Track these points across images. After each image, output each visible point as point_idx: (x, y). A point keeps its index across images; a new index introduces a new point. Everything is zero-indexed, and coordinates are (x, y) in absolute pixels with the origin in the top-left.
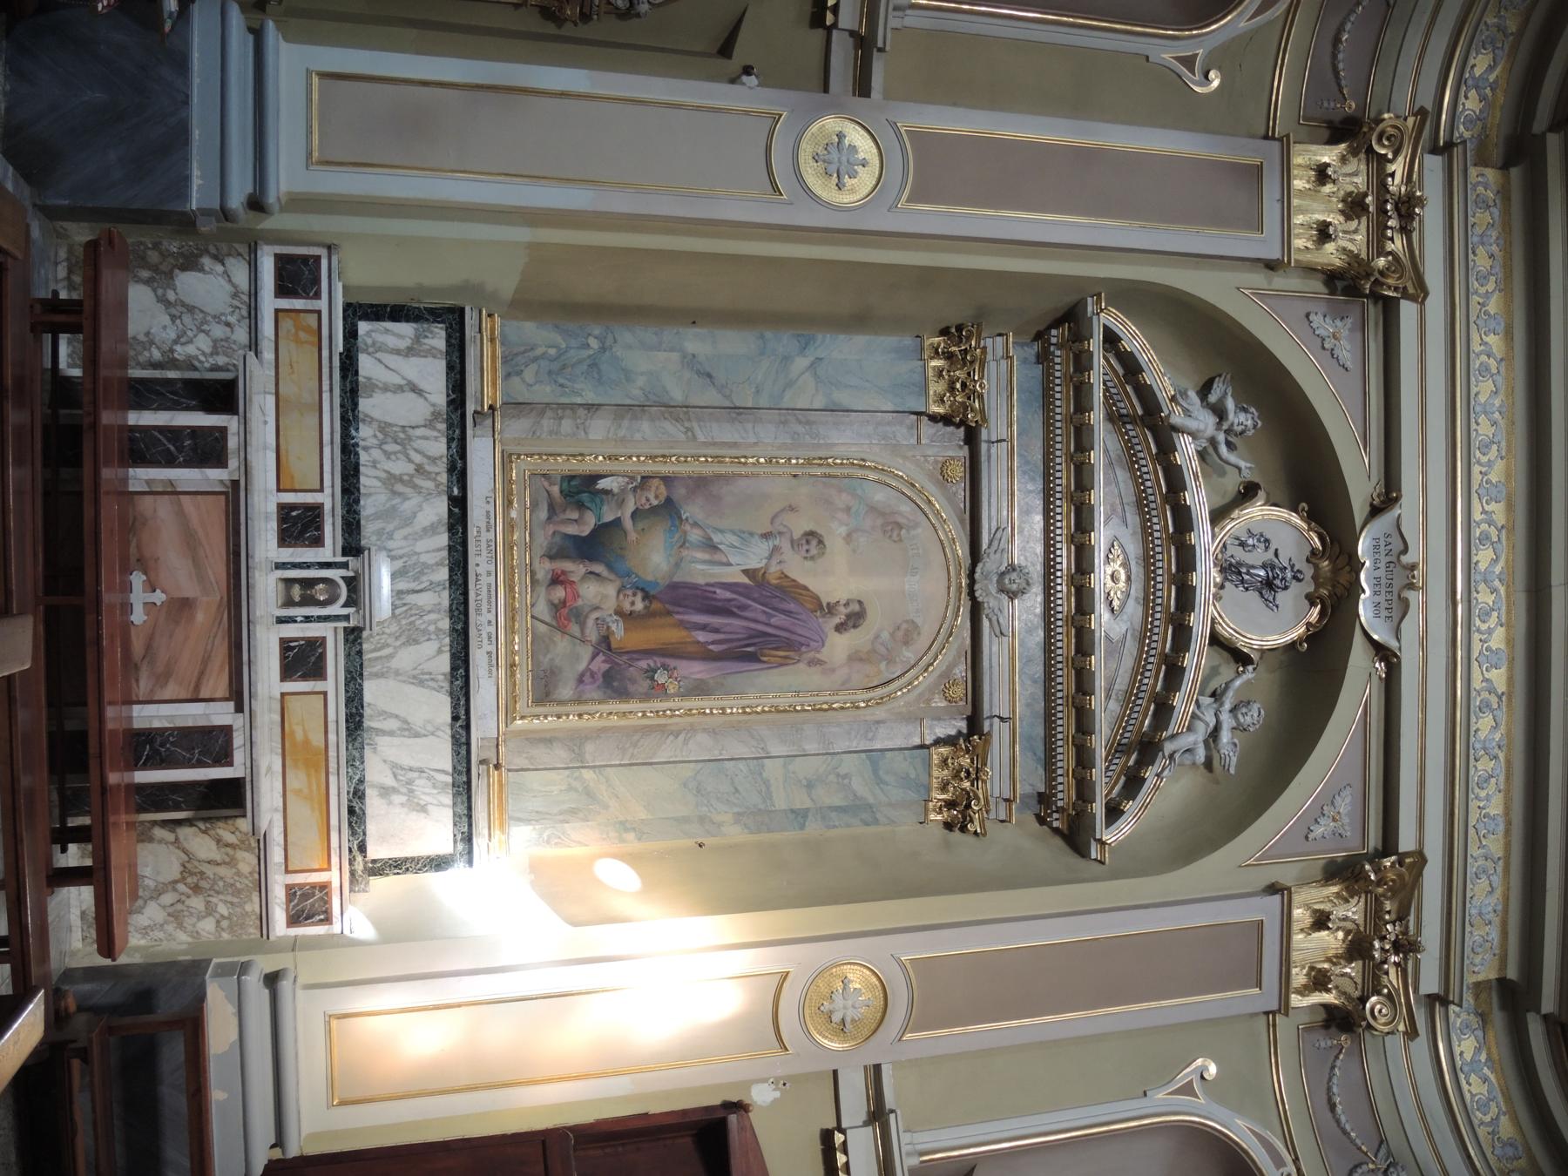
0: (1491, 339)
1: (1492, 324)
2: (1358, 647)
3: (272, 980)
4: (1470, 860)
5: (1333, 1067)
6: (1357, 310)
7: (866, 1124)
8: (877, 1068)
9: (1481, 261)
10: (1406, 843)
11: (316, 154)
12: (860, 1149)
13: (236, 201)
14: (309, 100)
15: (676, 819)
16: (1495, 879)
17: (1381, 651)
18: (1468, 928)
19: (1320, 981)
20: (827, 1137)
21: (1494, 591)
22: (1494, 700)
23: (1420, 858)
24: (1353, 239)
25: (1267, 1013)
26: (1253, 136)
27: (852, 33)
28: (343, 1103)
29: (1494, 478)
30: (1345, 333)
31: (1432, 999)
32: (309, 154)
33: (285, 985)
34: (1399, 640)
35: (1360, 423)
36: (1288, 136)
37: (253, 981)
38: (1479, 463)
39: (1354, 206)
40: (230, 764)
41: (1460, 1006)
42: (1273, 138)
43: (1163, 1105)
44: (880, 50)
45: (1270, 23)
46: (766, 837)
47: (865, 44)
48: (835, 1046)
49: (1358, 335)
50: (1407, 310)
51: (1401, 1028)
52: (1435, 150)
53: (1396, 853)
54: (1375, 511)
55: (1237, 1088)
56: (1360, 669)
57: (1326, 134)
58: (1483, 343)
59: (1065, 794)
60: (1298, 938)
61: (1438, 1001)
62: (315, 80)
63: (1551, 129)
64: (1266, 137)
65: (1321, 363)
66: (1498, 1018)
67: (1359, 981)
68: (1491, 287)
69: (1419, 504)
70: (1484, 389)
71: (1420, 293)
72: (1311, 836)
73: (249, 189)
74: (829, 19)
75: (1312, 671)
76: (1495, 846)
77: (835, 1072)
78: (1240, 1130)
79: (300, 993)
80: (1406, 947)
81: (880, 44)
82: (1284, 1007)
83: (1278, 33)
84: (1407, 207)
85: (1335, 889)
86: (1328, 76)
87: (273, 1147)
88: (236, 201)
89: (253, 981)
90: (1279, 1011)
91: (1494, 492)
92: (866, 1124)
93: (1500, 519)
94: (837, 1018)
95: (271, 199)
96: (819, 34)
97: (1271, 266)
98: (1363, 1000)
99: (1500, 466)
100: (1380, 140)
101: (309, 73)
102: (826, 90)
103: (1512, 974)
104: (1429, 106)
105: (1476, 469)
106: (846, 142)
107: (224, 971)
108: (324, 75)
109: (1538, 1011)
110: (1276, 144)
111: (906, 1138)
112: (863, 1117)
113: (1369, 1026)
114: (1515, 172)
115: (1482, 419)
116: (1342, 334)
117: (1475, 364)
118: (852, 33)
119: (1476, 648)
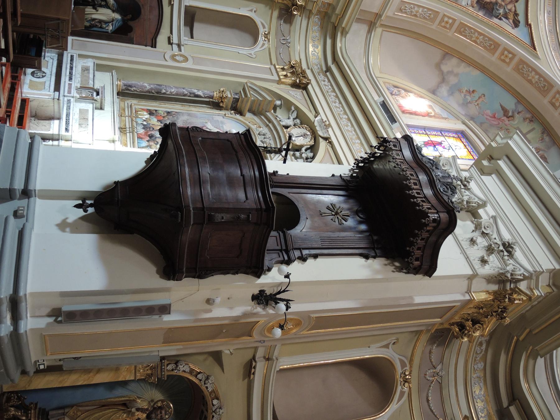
17: (326, 139)
63: (510, 405)
115: (478, 400)
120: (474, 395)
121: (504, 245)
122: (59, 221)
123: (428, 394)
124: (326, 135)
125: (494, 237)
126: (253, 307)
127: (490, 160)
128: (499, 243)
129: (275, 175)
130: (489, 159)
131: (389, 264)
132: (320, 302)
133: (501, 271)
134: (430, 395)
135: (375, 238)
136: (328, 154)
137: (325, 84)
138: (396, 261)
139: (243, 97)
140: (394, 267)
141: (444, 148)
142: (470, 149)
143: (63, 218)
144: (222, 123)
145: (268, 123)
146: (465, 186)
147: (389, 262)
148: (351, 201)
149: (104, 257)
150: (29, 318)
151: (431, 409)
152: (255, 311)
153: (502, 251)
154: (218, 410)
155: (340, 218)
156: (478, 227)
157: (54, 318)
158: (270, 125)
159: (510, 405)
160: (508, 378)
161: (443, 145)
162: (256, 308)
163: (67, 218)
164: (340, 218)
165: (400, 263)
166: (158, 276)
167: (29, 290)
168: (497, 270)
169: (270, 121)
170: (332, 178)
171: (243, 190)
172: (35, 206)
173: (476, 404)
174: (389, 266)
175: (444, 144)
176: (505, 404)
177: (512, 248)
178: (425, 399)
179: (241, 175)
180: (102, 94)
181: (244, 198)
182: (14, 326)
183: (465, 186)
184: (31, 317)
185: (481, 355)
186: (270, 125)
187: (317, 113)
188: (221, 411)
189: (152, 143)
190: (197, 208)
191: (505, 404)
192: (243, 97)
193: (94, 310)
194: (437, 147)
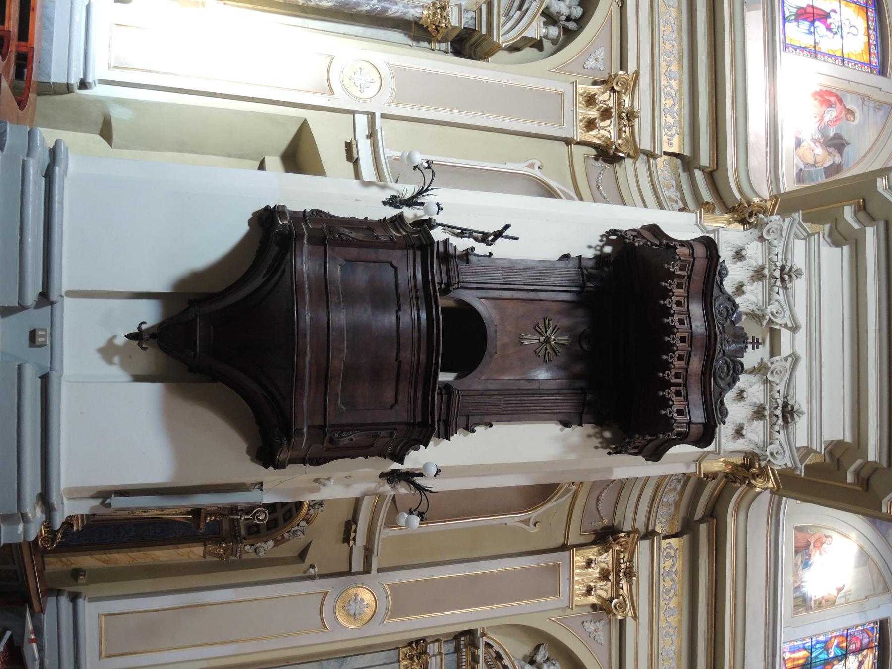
1: (672, 613)
4: (660, 629)
11: (103, 653)
14: (100, 628)
16: (674, 637)
21: (674, 118)
22: (671, 631)
23: (637, 73)
24: (604, 590)
29: (672, 605)
30: (600, 628)
32: (100, 654)
38: (666, 134)
46: (306, 276)
48: (352, 627)
49: (607, 626)
62: (103, 618)
68: (674, 132)
70: (666, 102)
76: (673, 620)
91: (673, 76)
93: (674, 624)
94: (352, 612)
99: (675, 599)
100: (617, 84)
101: (99, 616)
106: (359, 598)
108: (105, 615)
116: (599, 630)
121: (785, 405)
122: (102, 343)
123: (601, 493)
125: (777, 388)
126: (379, 483)
127: (859, 210)
128: (780, 402)
129: (467, 261)
130: (860, 206)
131: (595, 435)
132: (476, 476)
133: (757, 451)
134: (603, 494)
135: (589, 397)
136: (607, 27)
138: (605, 430)
140: (600, 440)
141: (828, 28)
142: (873, 41)
143: (109, 336)
146: (783, 280)
147: (596, 430)
148: (580, 312)
149: (171, 424)
150: (65, 502)
151: (598, 509)
152: (381, 489)
153: (777, 416)
154: (317, 507)
155: (549, 350)
156: (763, 370)
157: (100, 500)
160: (710, 505)
161: (829, 21)
162: (383, 485)
163: (115, 337)
164: (549, 350)
165: (613, 433)
166: (248, 458)
167: (64, 485)
168: (752, 446)
170: (563, 264)
171: (394, 384)
172: (62, 317)
174: (593, 438)
175: (834, 20)
176: (699, 514)
177: (793, 419)
178: (595, 497)
179: (397, 360)
181: (392, 400)
182: (46, 514)
183: (783, 280)
184: (69, 499)
188: (320, 509)
190: (314, 426)
191: (698, 515)
194: (817, 23)
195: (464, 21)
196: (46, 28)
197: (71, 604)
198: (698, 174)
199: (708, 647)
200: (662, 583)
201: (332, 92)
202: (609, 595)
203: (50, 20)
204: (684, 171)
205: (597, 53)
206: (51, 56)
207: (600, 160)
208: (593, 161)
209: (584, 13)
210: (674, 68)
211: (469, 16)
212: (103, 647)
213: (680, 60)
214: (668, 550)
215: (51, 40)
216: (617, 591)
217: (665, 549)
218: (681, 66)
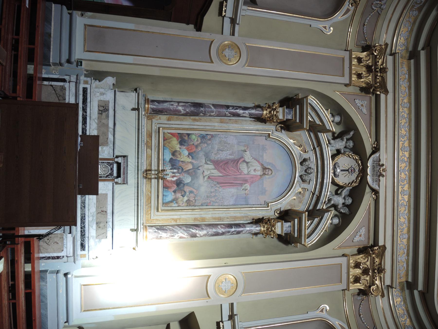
0: (405, 109)
2: (368, 190)
3: (66, 275)
5: (360, 304)
6: (368, 98)
7: (229, 320)
8: (232, 304)
9: (403, 132)
10: (381, 243)
12: (227, 326)
13: (63, 60)
15: (188, 226)
17: (373, 190)
18: (398, 263)
19: (357, 280)
20: (218, 324)
25: (343, 290)
26: (341, 50)
27: (230, 18)
28: (84, 311)
31: (388, 286)
33: (69, 276)
34: (379, 187)
35: (369, 130)
36: (351, 50)
37: (61, 275)
39: (369, 69)
40: (106, 195)
41: (396, 288)
42: (348, 51)
43: (315, 314)
44: (238, 24)
45: (347, 19)
47: (233, 21)
50: (383, 96)
51: (380, 294)
52: (391, 55)
53: (378, 245)
54: (373, 153)
55: (336, 311)
56: (368, 199)
57: (360, 49)
58: (401, 241)
59: (317, 193)
60: (351, 270)
61: (390, 287)
63: (423, 49)
64: (346, 50)
65: (358, 111)
66: (407, 292)
67: (369, 282)
68: (405, 182)
69: (384, 156)
71: (386, 92)
72: (354, 241)
73: (67, 58)
74: (224, 14)
75: (356, 193)
77: (221, 305)
78: (336, 322)
79: (74, 279)
80: (381, 270)
81: (238, 22)
82: (348, 289)
83: (349, 23)
84: (384, 70)
85: (361, 256)
86: (361, 33)
87: (65, 322)
88: (63, 60)
89: (61, 275)
90: (347, 290)
91: (406, 106)
92: (229, 320)
95: (73, 60)
96: (221, 18)
97: (346, 85)
98: (370, 287)
102: (222, 34)
103: (410, 280)
104: (389, 42)
105: (401, 143)
107: (52, 272)
108: (84, 285)
109: (417, 289)
110: (348, 52)
111: (240, 323)
112: (227, 318)
113: (372, 294)
114: (412, 61)
115: (401, 218)
117: (401, 115)
118: (230, 18)
119: (400, 190)
120: (400, 169)
124: (375, 187)
137: (403, 70)
139: (298, 121)
144: (264, 149)
145: (316, 146)
158: (317, 149)
159: (423, 49)
169: (319, 144)
173: (400, 131)
180: (124, 174)
185: (419, 5)
186: (317, 149)
187: (376, 150)
189: (179, 195)
192: (298, 121)
193: (169, 20)
195: (284, 229)
196: (43, 302)
197: (65, 278)
198: (416, 293)
199: (427, 192)
200: (400, 175)
201: (209, 297)
202: (369, 285)
203: (45, 297)
204: (408, 289)
205: (361, 231)
206: (47, 318)
207: (361, 295)
208: (356, 296)
209: (352, 203)
210: (406, 187)
211: (287, 226)
212: (83, 291)
213: (410, 139)
214: (403, 157)
215: (47, 308)
216: (373, 282)
217: (401, 200)
218: (410, 187)
